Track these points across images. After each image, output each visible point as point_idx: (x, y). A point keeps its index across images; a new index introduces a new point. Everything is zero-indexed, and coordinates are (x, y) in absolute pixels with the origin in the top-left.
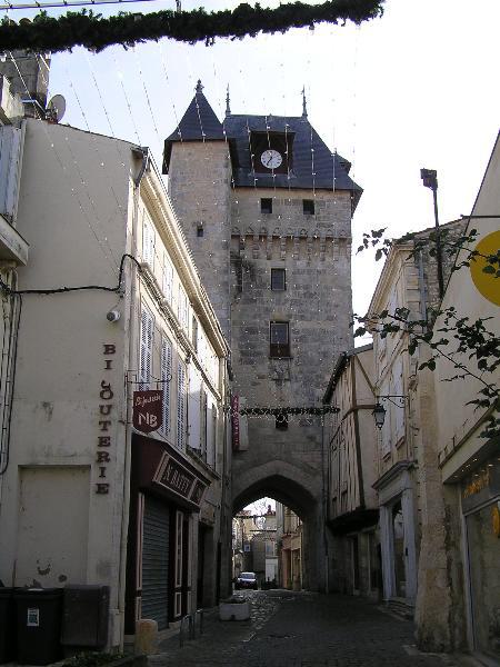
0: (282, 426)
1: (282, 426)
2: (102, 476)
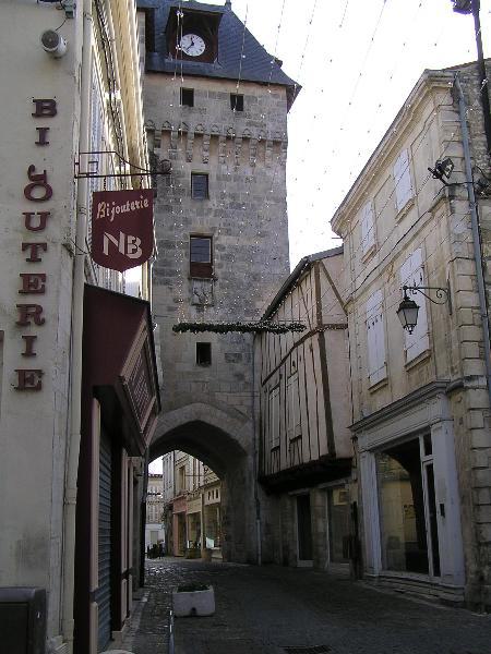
0: (204, 352)
1: (204, 352)
2: (29, 354)
